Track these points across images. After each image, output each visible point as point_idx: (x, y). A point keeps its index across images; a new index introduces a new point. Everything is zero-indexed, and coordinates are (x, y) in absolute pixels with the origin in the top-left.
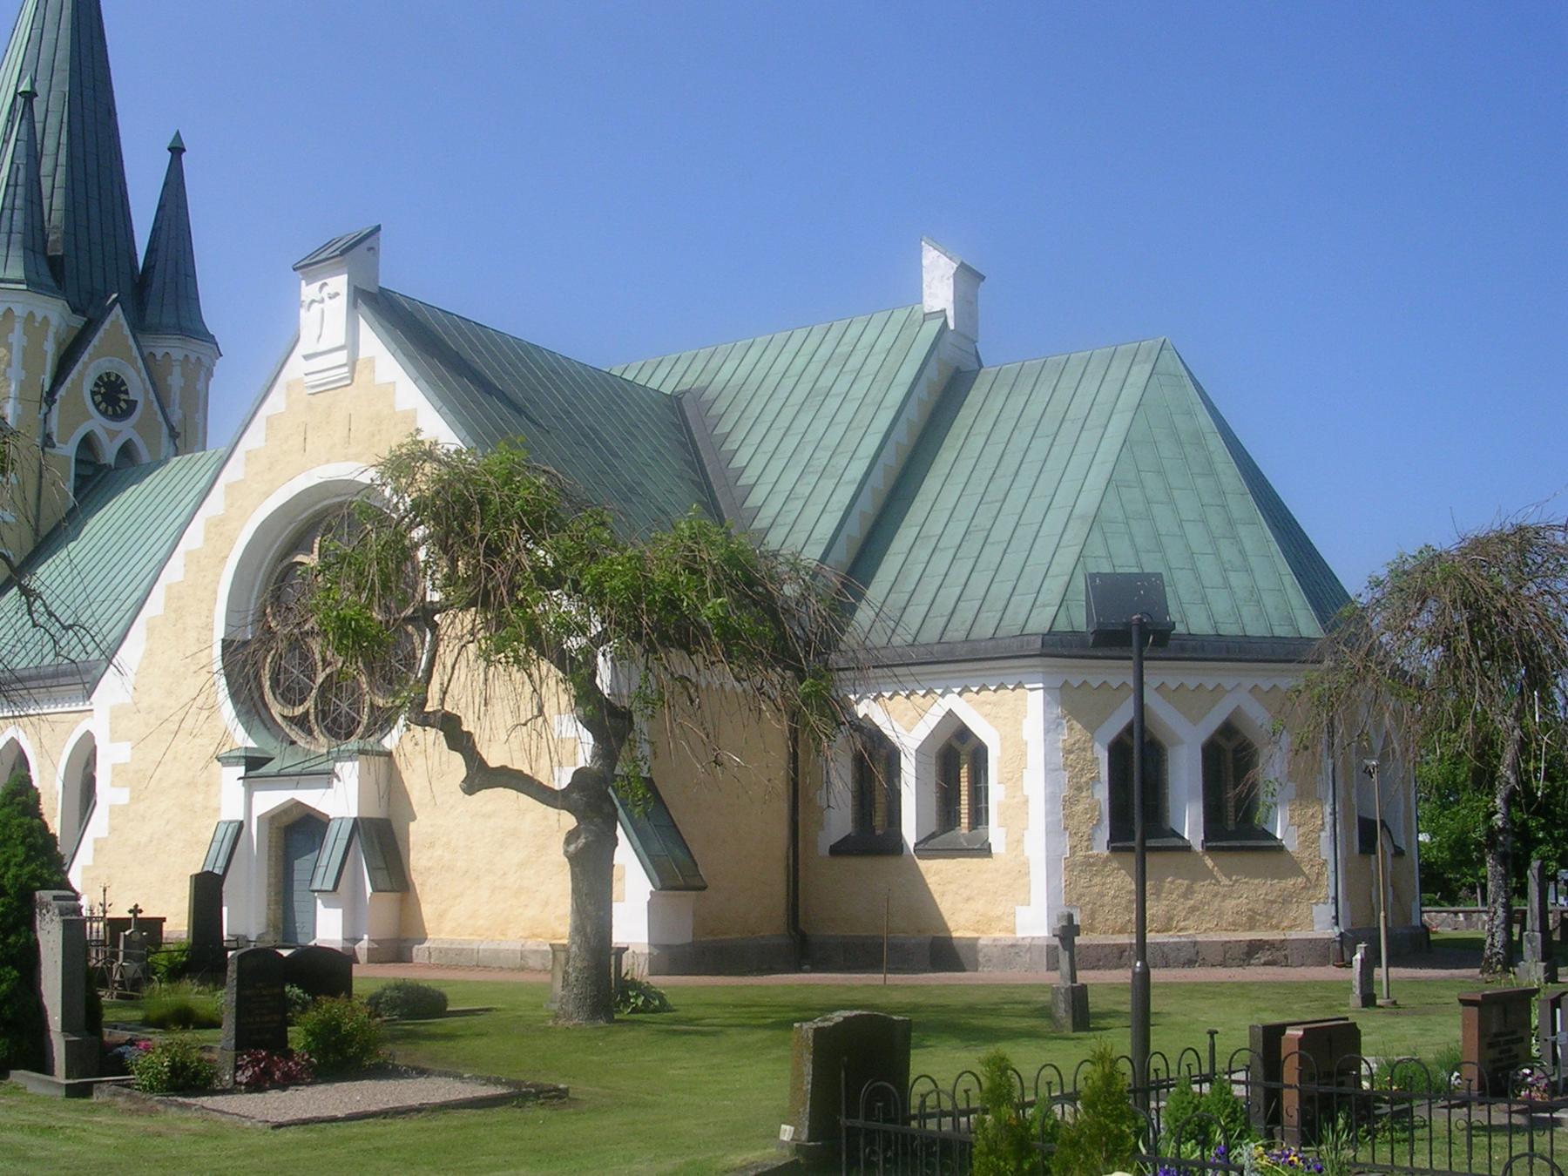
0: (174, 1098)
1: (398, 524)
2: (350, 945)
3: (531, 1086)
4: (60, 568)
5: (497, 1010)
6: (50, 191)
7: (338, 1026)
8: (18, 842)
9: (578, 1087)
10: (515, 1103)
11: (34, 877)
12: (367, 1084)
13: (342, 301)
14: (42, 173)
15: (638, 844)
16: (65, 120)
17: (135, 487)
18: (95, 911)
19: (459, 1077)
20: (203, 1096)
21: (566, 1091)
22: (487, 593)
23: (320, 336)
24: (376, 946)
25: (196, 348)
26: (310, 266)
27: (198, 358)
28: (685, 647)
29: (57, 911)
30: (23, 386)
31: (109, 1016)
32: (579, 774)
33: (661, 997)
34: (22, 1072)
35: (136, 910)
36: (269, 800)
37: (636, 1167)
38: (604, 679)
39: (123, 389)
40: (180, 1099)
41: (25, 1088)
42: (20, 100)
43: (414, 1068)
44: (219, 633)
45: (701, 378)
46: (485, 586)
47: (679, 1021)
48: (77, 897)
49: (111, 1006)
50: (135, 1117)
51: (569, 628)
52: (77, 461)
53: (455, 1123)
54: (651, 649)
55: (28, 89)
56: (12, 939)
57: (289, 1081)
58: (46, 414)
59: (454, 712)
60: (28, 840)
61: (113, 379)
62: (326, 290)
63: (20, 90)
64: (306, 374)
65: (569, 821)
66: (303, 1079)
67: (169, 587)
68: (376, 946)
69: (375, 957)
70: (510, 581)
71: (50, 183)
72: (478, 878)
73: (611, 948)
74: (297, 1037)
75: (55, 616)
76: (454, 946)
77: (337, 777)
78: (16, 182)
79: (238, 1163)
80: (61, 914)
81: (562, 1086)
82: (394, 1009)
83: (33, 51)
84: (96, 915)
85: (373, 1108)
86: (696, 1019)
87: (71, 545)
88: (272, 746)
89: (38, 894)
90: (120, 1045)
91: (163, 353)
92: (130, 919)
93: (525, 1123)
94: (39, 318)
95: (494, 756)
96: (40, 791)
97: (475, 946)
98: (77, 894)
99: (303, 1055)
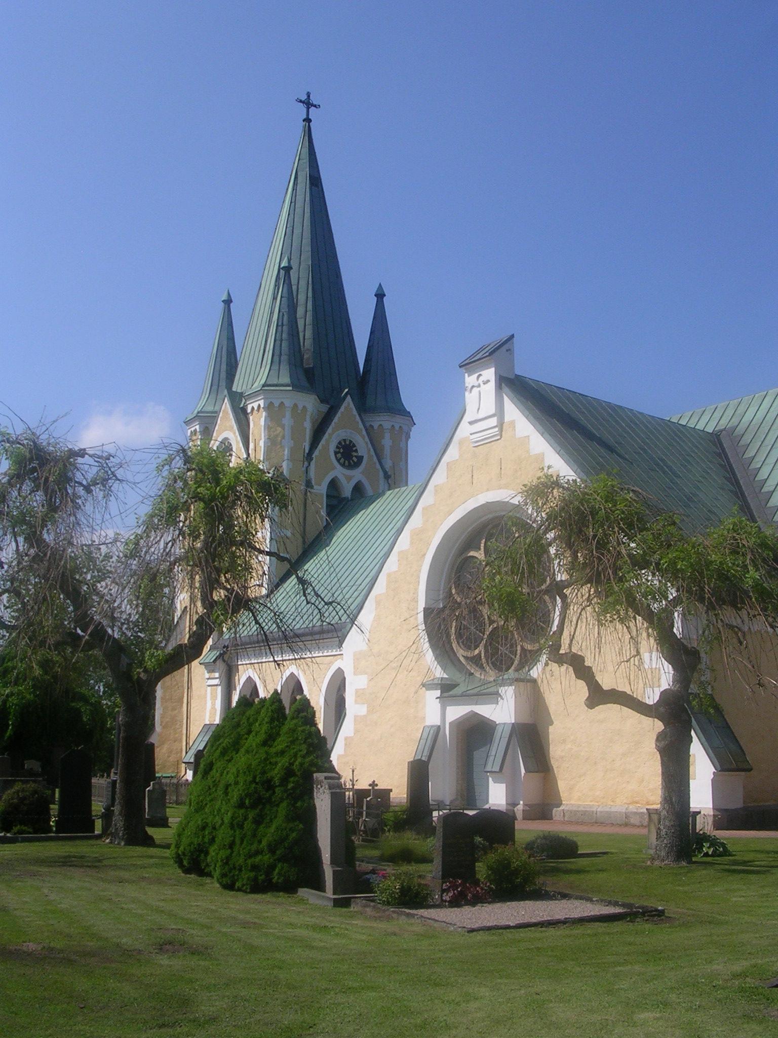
0: (403, 910)
1: (539, 529)
2: (511, 808)
3: (639, 907)
4: (323, 567)
5: (612, 853)
6: (303, 327)
7: (509, 864)
8: (302, 742)
9: (671, 909)
10: (628, 919)
11: (312, 764)
12: (529, 904)
13: (492, 385)
14: (298, 317)
15: (703, 739)
16: (310, 282)
17: (364, 511)
18: (347, 784)
19: (589, 900)
20: (421, 908)
21: (663, 912)
22: (599, 574)
23: (479, 409)
24: (528, 808)
25: (398, 421)
26: (471, 364)
27: (400, 427)
28: (734, 605)
29: (327, 787)
30: (292, 451)
31: (359, 853)
32: (663, 694)
33: (723, 845)
34: (305, 889)
35: (373, 784)
36: (456, 712)
37: (715, 967)
38: (678, 629)
39: (354, 449)
40: (407, 911)
41: (308, 900)
42: (282, 272)
43: (559, 893)
44: (422, 605)
45: (732, 421)
46: (598, 568)
47: (735, 863)
48: (339, 777)
49: (362, 846)
50: (378, 921)
51: (651, 593)
52: (328, 496)
53: (589, 932)
54: (711, 607)
55: (287, 265)
56: (299, 804)
57: (476, 900)
58: (307, 468)
59: (579, 653)
60: (309, 740)
61: (348, 443)
62: (481, 379)
63: (282, 265)
64: (471, 434)
65: (659, 726)
66: (486, 899)
67: (389, 575)
68: (528, 808)
69: (527, 816)
70: (614, 564)
71: (303, 322)
72: (595, 763)
73: (690, 812)
74: (482, 871)
75: (321, 598)
76: (580, 809)
77: (500, 696)
78: (282, 323)
79: (447, 955)
80: (330, 788)
81: (660, 908)
82: (543, 852)
83: (288, 241)
84: (348, 787)
85: (533, 920)
86: (748, 862)
87: (327, 548)
88: (458, 677)
89: (315, 775)
90: (367, 873)
91: (378, 425)
92: (370, 790)
93: (636, 934)
94: (300, 407)
95: (606, 681)
96: (315, 709)
97: (594, 809)
98: (339, 775)
99: (486, 884)
